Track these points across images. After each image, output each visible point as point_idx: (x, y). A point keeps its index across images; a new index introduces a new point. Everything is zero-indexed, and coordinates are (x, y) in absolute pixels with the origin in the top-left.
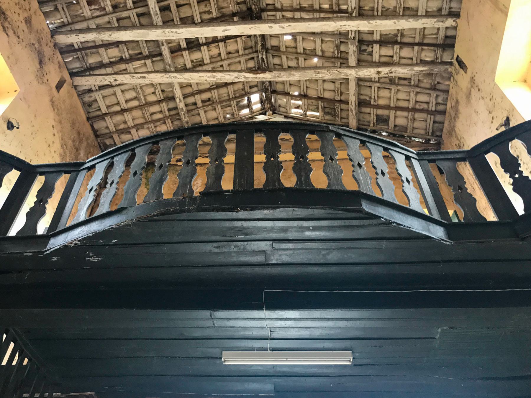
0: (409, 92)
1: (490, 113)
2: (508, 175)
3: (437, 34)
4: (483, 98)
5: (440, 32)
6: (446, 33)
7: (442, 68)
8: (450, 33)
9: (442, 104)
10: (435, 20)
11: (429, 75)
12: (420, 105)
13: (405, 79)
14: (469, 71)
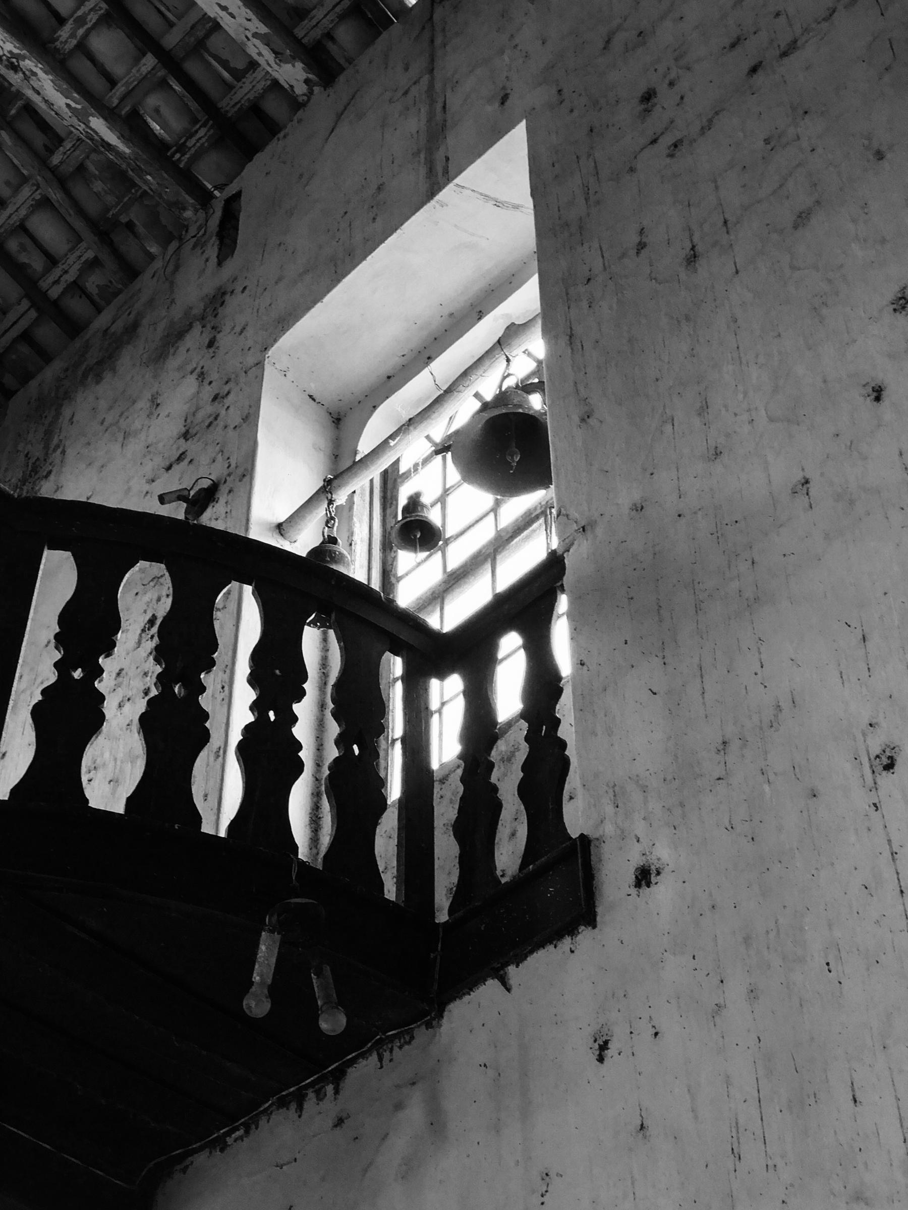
0: (24, 180)
1: (186, 436)
2: (58, 656)
3: (239, 75)
4: (202, 376)
5: (250, 77)
6: (262, 96)
7: (172, 191)
8: (274, 107)
9: (89, 297)
10: (263, 29)
11: (118, 175)
12: (23, 248)
13: (43, 125)
14: (231, 266)
